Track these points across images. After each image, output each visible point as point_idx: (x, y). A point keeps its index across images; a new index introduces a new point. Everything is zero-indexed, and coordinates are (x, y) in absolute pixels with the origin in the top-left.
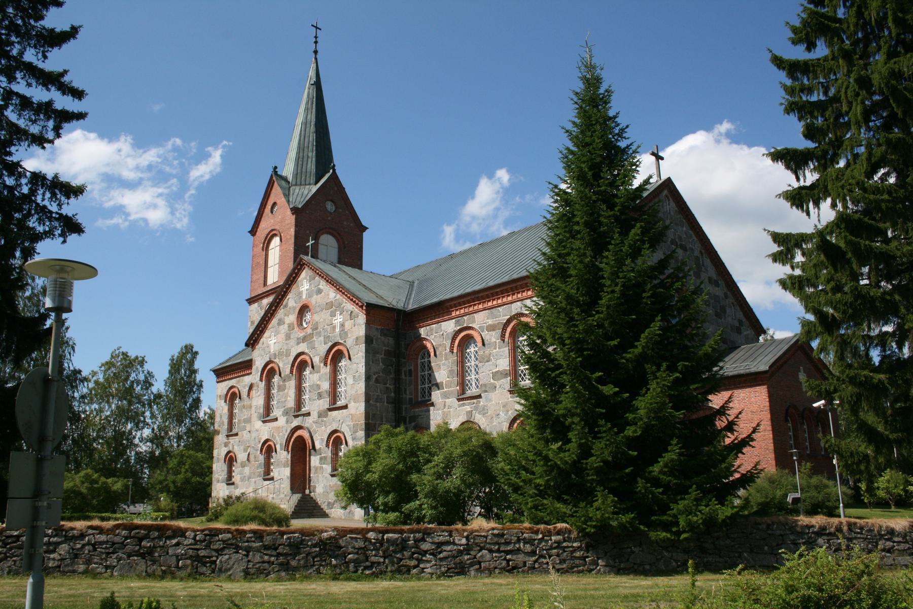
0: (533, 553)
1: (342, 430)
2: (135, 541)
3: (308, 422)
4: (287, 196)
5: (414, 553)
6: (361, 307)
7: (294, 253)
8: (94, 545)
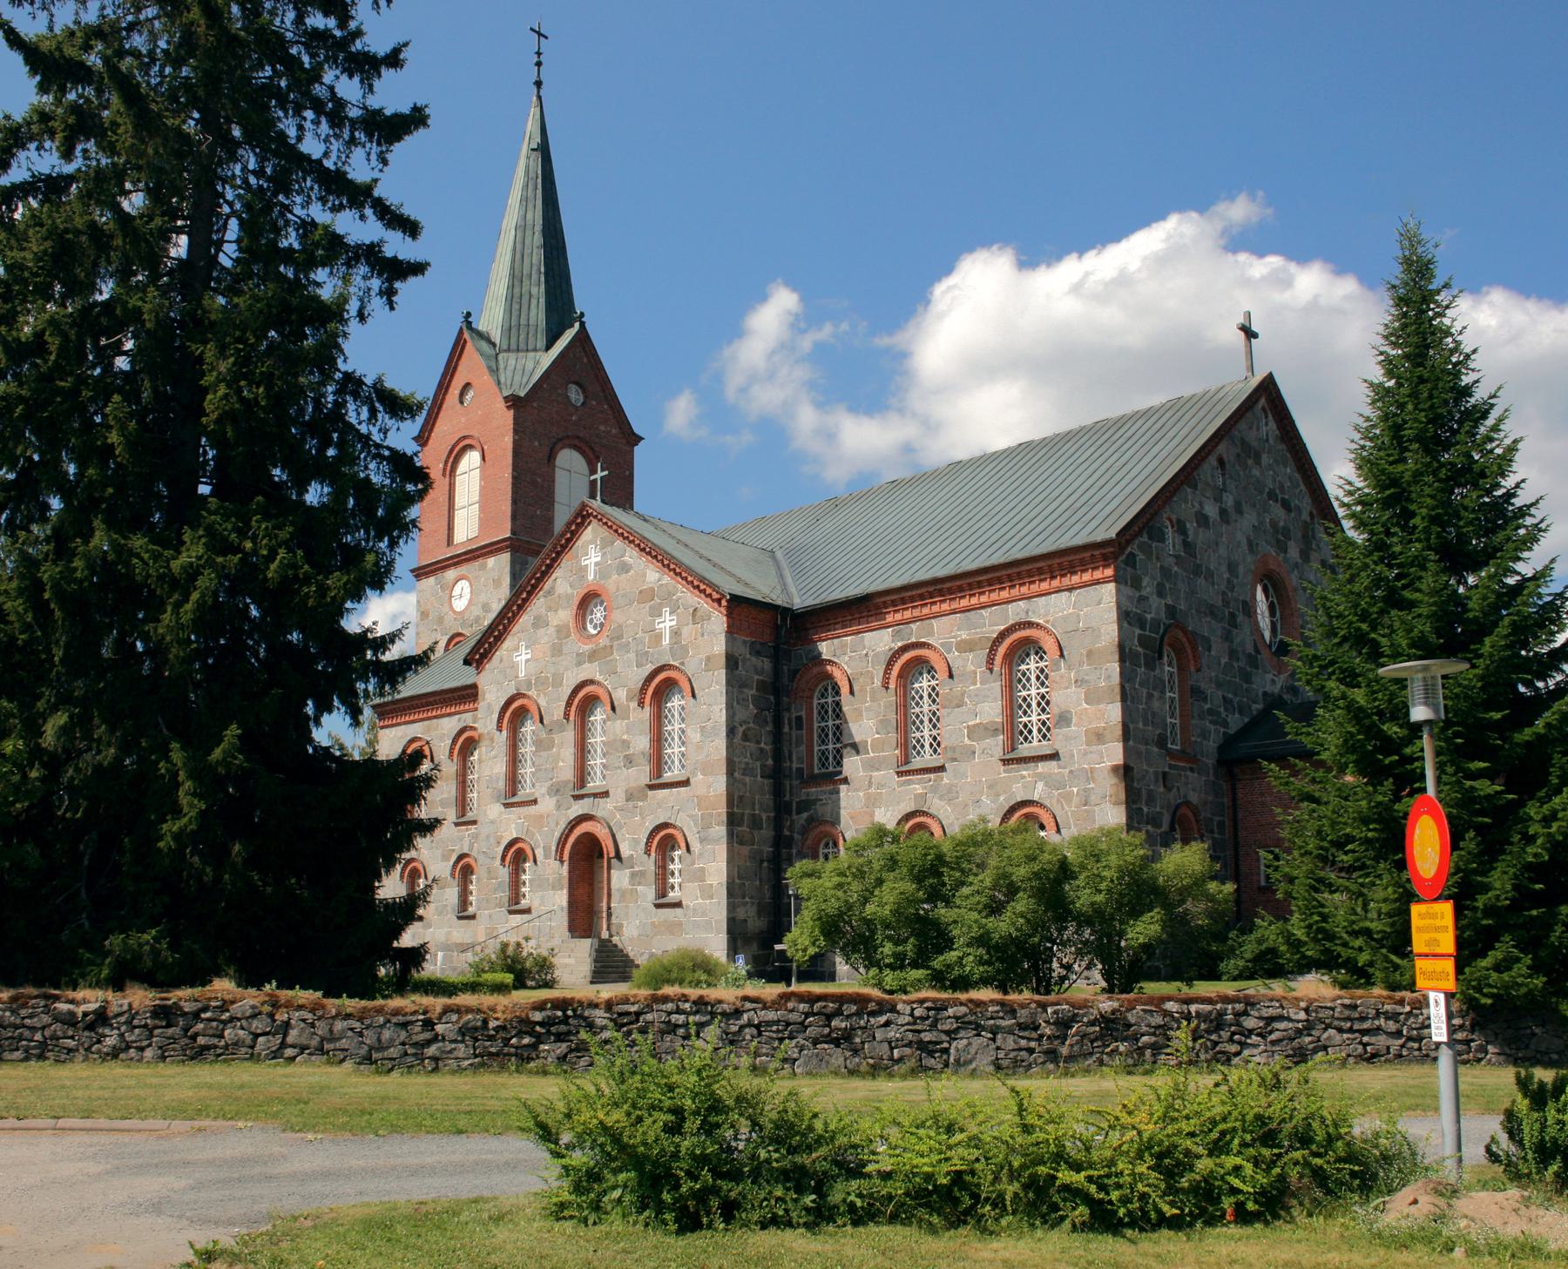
0: (1398, 1034)
1: (678, 824)
2: (822, 1020)
3: (603, 808)
4: (494, 371)
5: (1233, 1034)
6: (719, 601)
7: (513, 484)
8: (758, 1027)
